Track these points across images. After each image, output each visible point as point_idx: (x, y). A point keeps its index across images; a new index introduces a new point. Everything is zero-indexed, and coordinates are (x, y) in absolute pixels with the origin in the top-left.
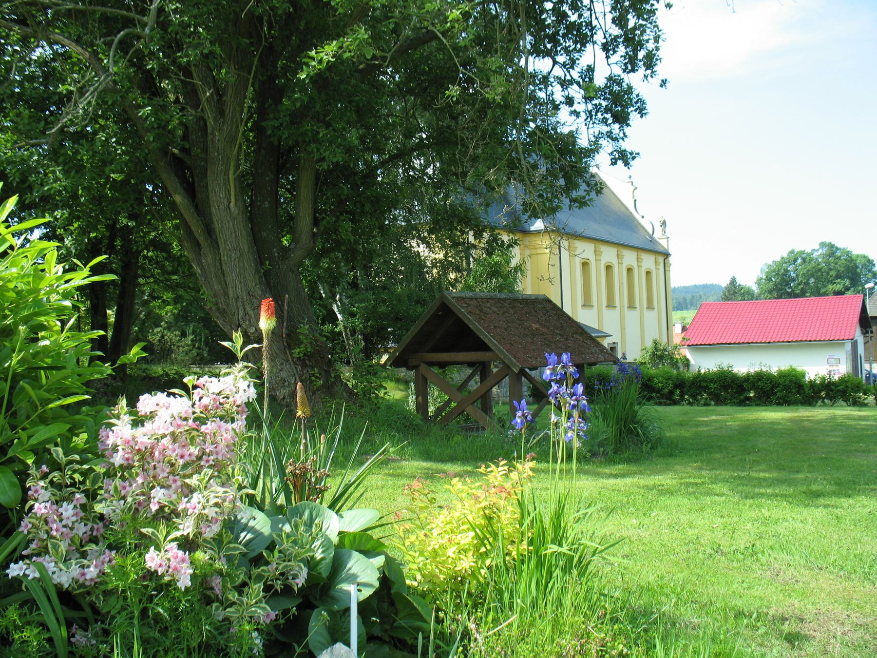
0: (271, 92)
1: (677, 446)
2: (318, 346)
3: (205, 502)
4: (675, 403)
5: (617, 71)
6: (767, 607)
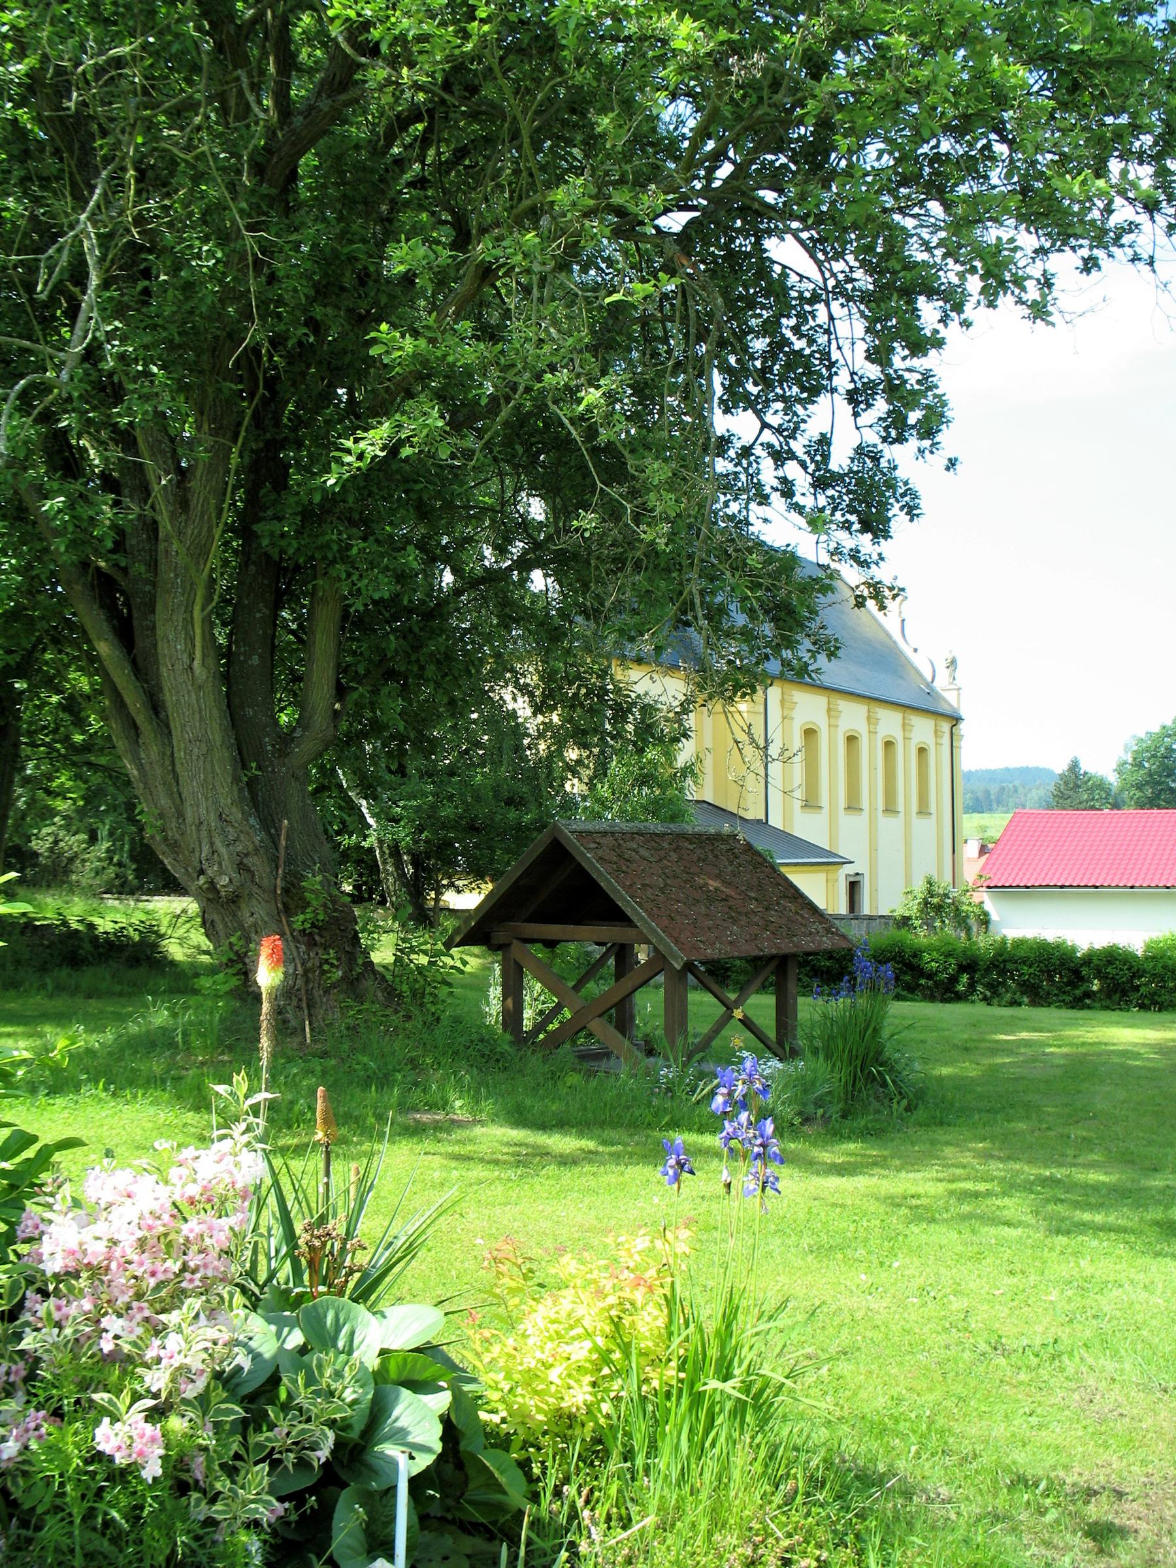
0: (266, 473)
1: (952, 1104)
2: (336, 910)
3: (187, 1348)
4: (959, 998)
5: (872, 437)
6: (1066, 1468)
